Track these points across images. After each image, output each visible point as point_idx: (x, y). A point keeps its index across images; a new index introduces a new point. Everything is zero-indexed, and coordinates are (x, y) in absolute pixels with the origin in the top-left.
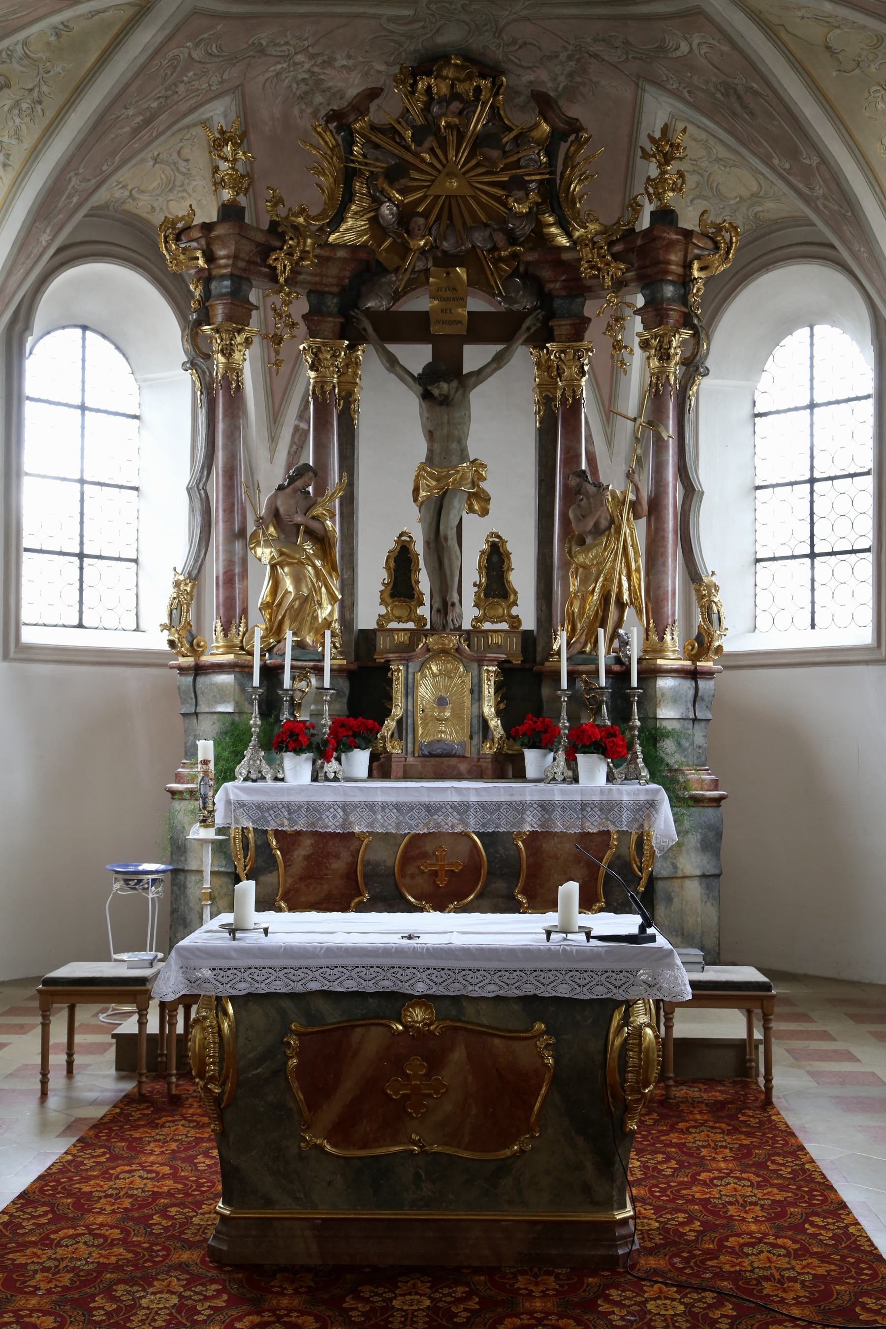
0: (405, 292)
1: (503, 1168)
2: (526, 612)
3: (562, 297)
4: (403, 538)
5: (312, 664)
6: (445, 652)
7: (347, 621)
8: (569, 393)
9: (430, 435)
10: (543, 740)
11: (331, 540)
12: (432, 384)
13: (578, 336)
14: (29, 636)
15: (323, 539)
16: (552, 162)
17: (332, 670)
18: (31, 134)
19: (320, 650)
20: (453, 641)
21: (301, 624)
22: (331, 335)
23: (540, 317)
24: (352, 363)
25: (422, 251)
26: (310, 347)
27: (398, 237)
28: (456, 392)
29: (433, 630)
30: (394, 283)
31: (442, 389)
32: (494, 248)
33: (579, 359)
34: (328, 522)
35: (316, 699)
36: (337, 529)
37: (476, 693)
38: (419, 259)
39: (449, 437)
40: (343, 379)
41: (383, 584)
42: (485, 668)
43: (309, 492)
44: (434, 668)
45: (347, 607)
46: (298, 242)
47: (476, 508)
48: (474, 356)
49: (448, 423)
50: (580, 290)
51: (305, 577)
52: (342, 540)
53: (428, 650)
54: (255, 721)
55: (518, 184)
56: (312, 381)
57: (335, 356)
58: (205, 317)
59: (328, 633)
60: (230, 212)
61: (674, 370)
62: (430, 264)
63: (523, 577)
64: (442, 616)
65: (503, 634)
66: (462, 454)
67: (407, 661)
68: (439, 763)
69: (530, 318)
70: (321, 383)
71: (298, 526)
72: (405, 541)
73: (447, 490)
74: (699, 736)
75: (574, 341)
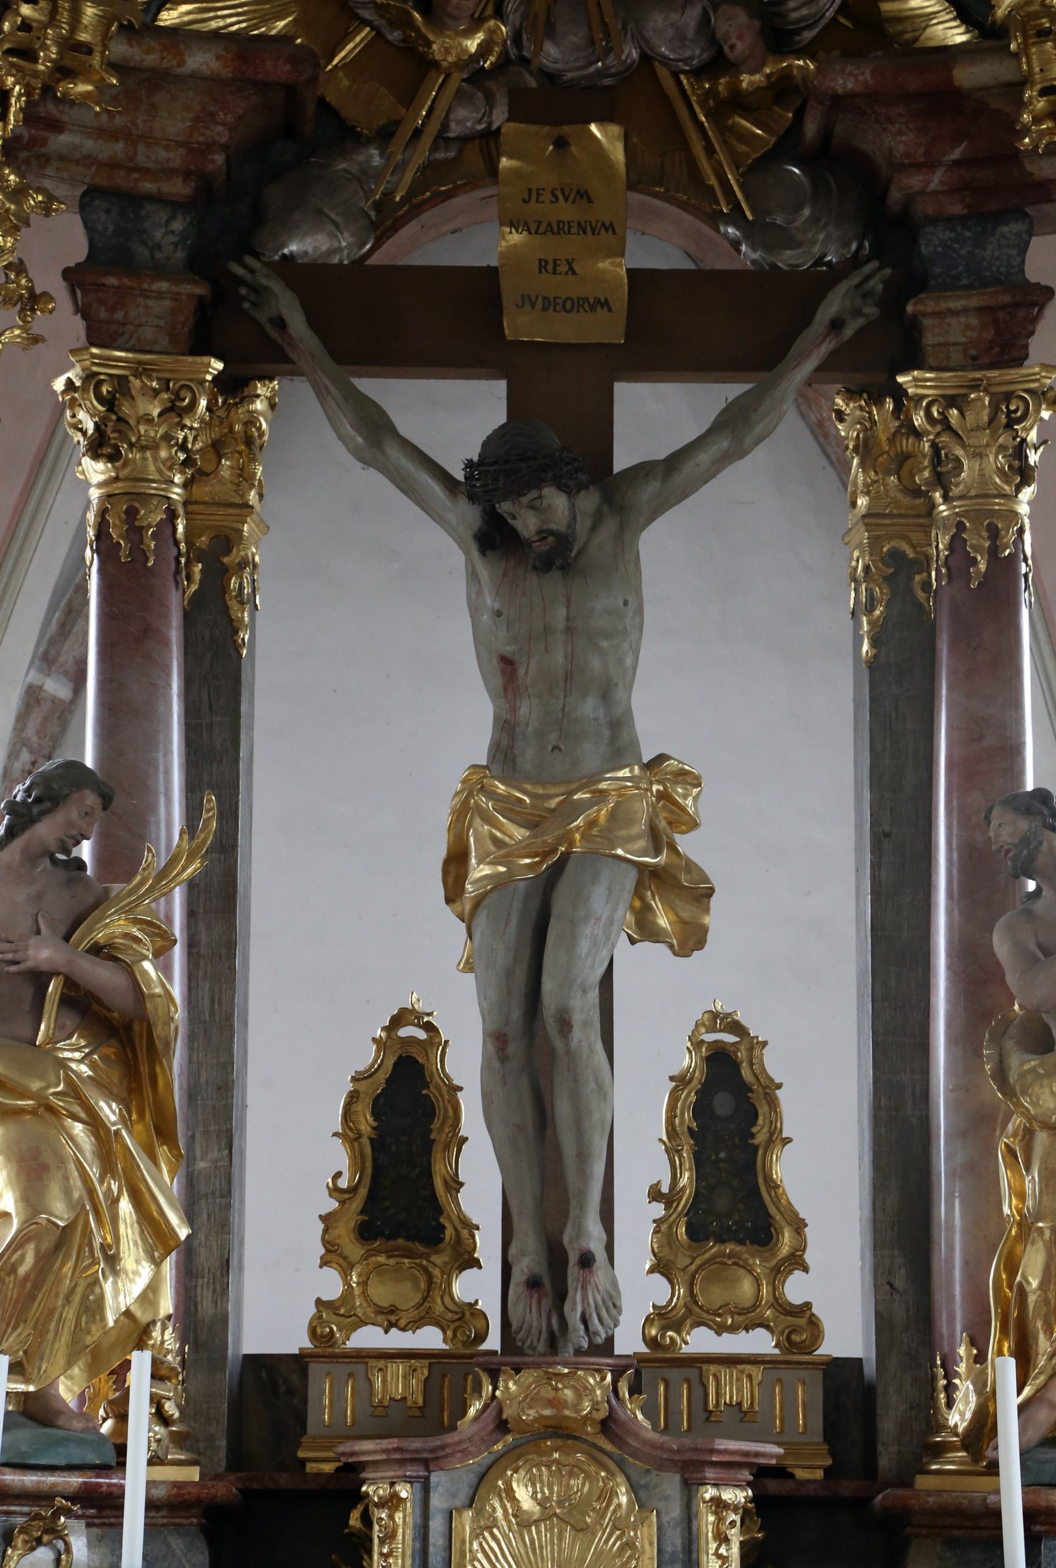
0: (415, 207)
2: (837, 1294)
3: (949, 221)
4: (405, 1032)
5: (75, 1480)
6: (560, 1431)
7: (203, 1318)
8: (976, 540)
9: (506, 673)
11: (158, 1031)
12: (515, 492)
13: (1006, 345)
15: (128, 1028)
17: (151, 1505)
19: (106, 1427)
20: (591, 1391)
21: (40, 1332)
22: (164, 341)
23: (876, 285)
24: (233, 441)
25: (476, 76)
26: (89, 377)
27: (393, 25)
28: (594, 528)
30: (378, 175)
31: (544, 518)
32: (718, 63)
33: (1009, 425)
34: (147, 965)
36: (177, 991)
38: (461, 97)
39: (571, 679)
40: (202, 491)
41: (335, 1191)
42: (709, 1493)
43: (80, 865)
44: (523, 1494)
45: (206, 1271)
46: (54, 13)
47: (663, 921)
48: (652, 416)
49: (569, 630)
51: (62, 1161)
52: (191, 1038)
53: (502, 1426)
56: (95, 494)
57: (176, 411)
59: (141, 1362)
62: (499, 116)
63: (821, 1166)
64: (547, 1302)
65: (757, 1373)
66: (614, 738)
67: (424, 1466)
69: (844, 287)
70: (125, 503)
71: (39, 979)
72: (412, 1040)
73: (565, 857)
75: (991, 366)
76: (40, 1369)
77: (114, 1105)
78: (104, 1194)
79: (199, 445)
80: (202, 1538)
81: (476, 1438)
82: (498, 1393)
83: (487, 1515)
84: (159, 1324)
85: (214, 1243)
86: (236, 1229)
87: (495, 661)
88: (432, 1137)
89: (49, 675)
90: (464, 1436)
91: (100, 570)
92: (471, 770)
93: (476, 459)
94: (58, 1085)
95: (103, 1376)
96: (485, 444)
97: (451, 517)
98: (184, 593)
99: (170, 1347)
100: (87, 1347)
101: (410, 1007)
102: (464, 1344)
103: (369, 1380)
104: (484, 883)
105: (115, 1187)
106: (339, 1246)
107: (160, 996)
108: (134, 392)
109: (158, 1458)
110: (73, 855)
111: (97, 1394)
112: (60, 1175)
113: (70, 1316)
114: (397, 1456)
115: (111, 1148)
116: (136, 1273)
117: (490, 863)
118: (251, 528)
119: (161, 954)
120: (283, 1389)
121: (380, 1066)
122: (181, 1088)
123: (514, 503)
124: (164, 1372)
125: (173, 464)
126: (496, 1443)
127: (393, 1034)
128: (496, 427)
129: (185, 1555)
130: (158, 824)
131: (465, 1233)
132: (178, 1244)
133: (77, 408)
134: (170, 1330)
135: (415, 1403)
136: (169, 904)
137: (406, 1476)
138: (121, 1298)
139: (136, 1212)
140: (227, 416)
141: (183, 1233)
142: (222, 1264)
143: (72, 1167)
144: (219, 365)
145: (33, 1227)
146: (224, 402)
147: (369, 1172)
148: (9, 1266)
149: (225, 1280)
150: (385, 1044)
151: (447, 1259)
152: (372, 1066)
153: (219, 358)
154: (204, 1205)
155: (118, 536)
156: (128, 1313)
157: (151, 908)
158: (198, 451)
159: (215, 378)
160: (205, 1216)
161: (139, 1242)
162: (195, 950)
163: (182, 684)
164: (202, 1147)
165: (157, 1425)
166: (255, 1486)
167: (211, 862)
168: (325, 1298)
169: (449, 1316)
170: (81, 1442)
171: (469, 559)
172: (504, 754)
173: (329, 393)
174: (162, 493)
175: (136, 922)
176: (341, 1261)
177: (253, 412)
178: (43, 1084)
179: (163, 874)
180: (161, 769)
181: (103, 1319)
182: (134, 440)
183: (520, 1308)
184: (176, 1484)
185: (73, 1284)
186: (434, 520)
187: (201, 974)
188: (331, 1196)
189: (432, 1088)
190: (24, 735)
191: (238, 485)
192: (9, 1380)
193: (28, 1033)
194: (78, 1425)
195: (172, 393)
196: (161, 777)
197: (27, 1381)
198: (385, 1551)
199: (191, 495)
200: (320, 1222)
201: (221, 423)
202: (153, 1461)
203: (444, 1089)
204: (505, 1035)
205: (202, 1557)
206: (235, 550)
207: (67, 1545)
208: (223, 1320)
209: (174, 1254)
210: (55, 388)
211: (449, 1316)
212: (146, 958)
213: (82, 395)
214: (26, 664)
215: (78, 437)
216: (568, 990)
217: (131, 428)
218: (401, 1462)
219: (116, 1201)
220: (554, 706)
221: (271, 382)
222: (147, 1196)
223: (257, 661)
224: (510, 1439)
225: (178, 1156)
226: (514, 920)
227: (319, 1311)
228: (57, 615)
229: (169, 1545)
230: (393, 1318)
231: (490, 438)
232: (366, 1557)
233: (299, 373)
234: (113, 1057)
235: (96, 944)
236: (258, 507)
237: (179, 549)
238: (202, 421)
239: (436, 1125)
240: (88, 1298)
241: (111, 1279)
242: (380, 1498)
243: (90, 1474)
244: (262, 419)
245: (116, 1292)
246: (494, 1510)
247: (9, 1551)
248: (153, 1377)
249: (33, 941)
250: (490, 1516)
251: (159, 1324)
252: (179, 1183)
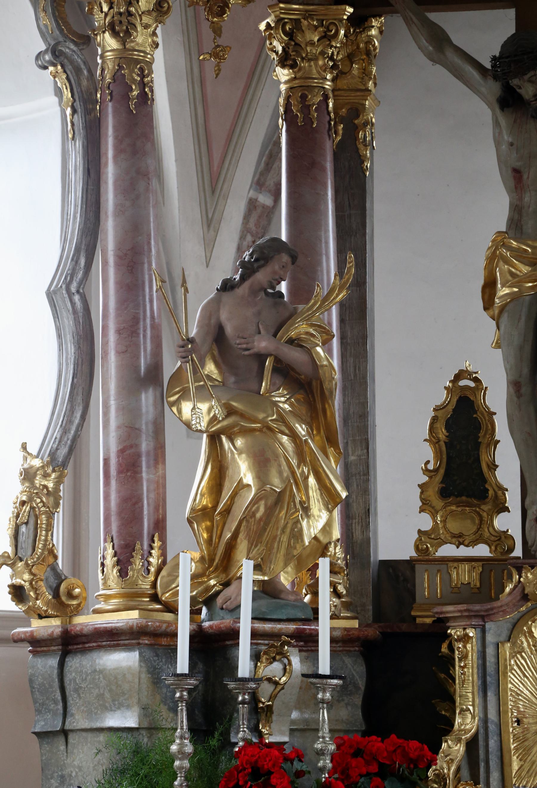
4: (463, 383)
5: (292, 627)
11: (326, 385)
15: (310, 384)
17: (333, 640)
19: (307, 599)
21: (269, 549)
24: (360, 53)
26: (279, 21)
34: (319, 349)
36: (335, 363)
41: (426, 471)
43: (281, 295)
45: (357, 515)
51: (277, 456)
52: (344, 389)
53: (525, 598)
54: (181, 745)
56: (283, 87)
57: (327, 37)
59: (324, 564)
67: (482, 619)
70: (300, 91)
71: (261, 358)
72: (467, 387)
76: (270, 568)
77: (304, 426)
78: (300, 475)
79: (340, 57)
80: (361, 658)
81: (511, 604)
82: (522, 579)
83: (518, 646)
84: (333, 544)
85: (361, 500)
86: (372, 493)
87: (510, 172)
88: (480, 440)
89: (261, 193)
90: (503, 603)
91: (287, 131)
92: (497, 235)
93: (497, 55)
94: (273, 415)
95: (304, 572)
96: (503, 46)
97: (483, 90)
98: (334, 141)
99: (339, 556)
100: (295, 556)
101: (465, 369)
102: (502, 554)
103: (449, 573)
104: (506, 298)
105: (306, 470)
106: (429, 501)
107: (326, 366)
108: (304, 28)
109: (336, 615)
110: (277, 290)
111: (301, 581)
112: (276, 464)
113: (285, 539)
114: (466, 614)
115: (303, 449)
116: (319, 516)
117: (509, 287)
118: (370, 103)
119: (326, 343)
120: (402, 578)
121: (449, 402)
122: (339, 416)
123: (520, 80)
124: (337, 569)
125: (326, 68)
126: (522, 606)
127: (456, 384)
128: (509, 35)
129: (353, 667)
130: (322, 271)
131: (500, 493)
132: (341, 500)
133: (273, 39)
134: (339, 547)
135: (475, 585)
136: (330, 315)
137: (472, 625)
138: (312, 530)
139: (318, 484)
140: (356, 39)
141: (344, 494)
142: (366, 512)
143: (282, 460)
144: (351, 10)
145: (263, 492)
146: (354, 31)
147: (445, 460)
148: (251, 513)
149: (368, 520)
150: (451, 390)
151: (490, 507)
152: (445, 402)
153: (351, 6)
154: (354, 480)
155: (297, 111)
156: (316, 538)
157: (320, 319)
158: (340, 60)
159: (349, 17)
160: (355, 486)
161: (320, 500)
162: (345, 341)
163: (334, 193)
164: (352, 448)
165: (334, 598)
166: (389, 631)
167: (352, 291)
168: (423, 529)
169: (493, 538)
170: (294, 607)
171: (494, 114)
172: (516, 224)
173: (413, 22)
174: (320, 85)
175: (312, 325)
176: (431, 509)
177: (370, 36)
178: (265, 415)
179: (326, 299)
180: (323, 241)
181: (303, 541)
182: (304, 55)
183: (533, 533)
184: (346, 629)
185: (286, 522)
186: (474, 92)
187: (348, 354)
188: (424, 474)
189: (478, 414)
190: (248, 226)
191: (362, 79)
192: (254, 574)
193: (255, 387)
194: (292, 597)
195: (325, 28)
196: (323, 245)
197: (264, 574)
198: (462, 665)
199: (336, 85)
200: (419, 488)
201: (353, 43)
202: (333, 617)
203: (486, 414)
204: (519, 382)
205: (362, 668)
206: (361, 116)
207: (289, 661)
208: (368, 541)
209: (339, 506)
210: (260, 28)
211: (493, 538)
212: (318, 345)
213: (275, 32)
214: (248, 187)
215: (274, 56)
217: (302, 49)
218: (469, 617)
219: (307, 478)
221: (380, 18)
222: (323, 475)
223: (375, 181)
224: (529, 604)
225: (339, 453)
226: (523, 318)
227: (420, 536)
228: (264, 159)
229: (344, 662)
230: (461, 540)
231: (506, 42)
232: (451, 668)
233: (396, 12)
234: (302, 400)
235: (291, 338)
236: (373, 91)
237: (330, 117)
238: (342, 42)
239: (481, 434)
240: (294, 530)
241: (306, 520)
242: (458, 636)
243: (299, 623)
244: (375, 40)
245: (309, 526)
246: (522, 643)
247: (259, 664)
248: (331, 572)
249: (257, 337)
250: (520, 646)
251: (333, 544)
252: (340, 468)
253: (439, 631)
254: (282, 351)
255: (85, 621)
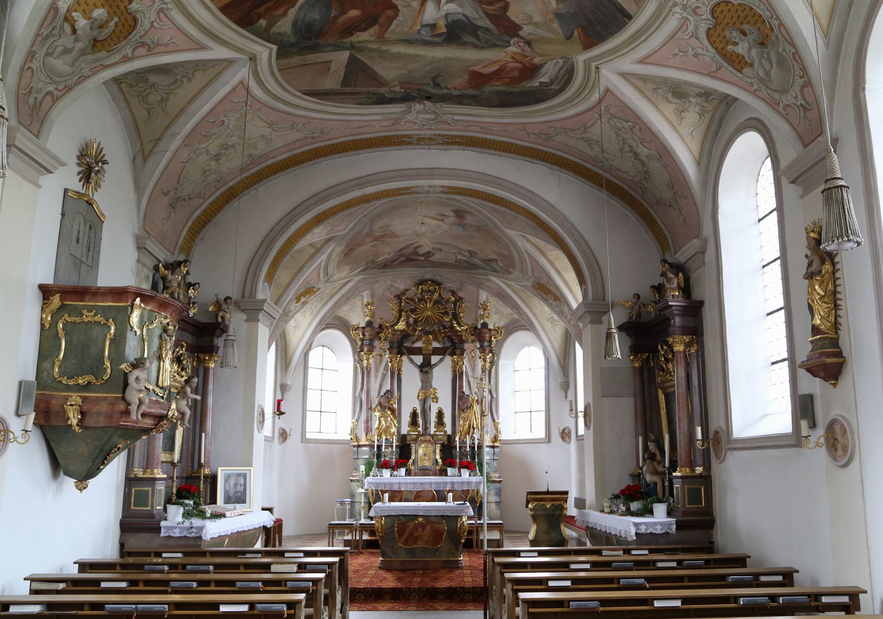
1: (437, 550)
2: (449, 430)
7: (399, 432)
9: (422, 381)
10: (452, 465)
14: (308, 436)
16: (455, 307)
18: (319, 305)
29: (423, 435)
31: (426, 368)
35: (391, 454)
37: (435, 452)
45: (399, 429)
48: (434, 359)
50: (462, 342)
54: (375, 460)
55: (446, 313)
58: (362, 350)
60: (369, 324)
61: (488, 365)
68: (424, 471)
70: (392, 367)
74: (495, 464)
172: (422, 388)
216: (427, 407)
220: (426, 384)
253: (410, 445)
254: (388, 404)
255: (361, 443)
